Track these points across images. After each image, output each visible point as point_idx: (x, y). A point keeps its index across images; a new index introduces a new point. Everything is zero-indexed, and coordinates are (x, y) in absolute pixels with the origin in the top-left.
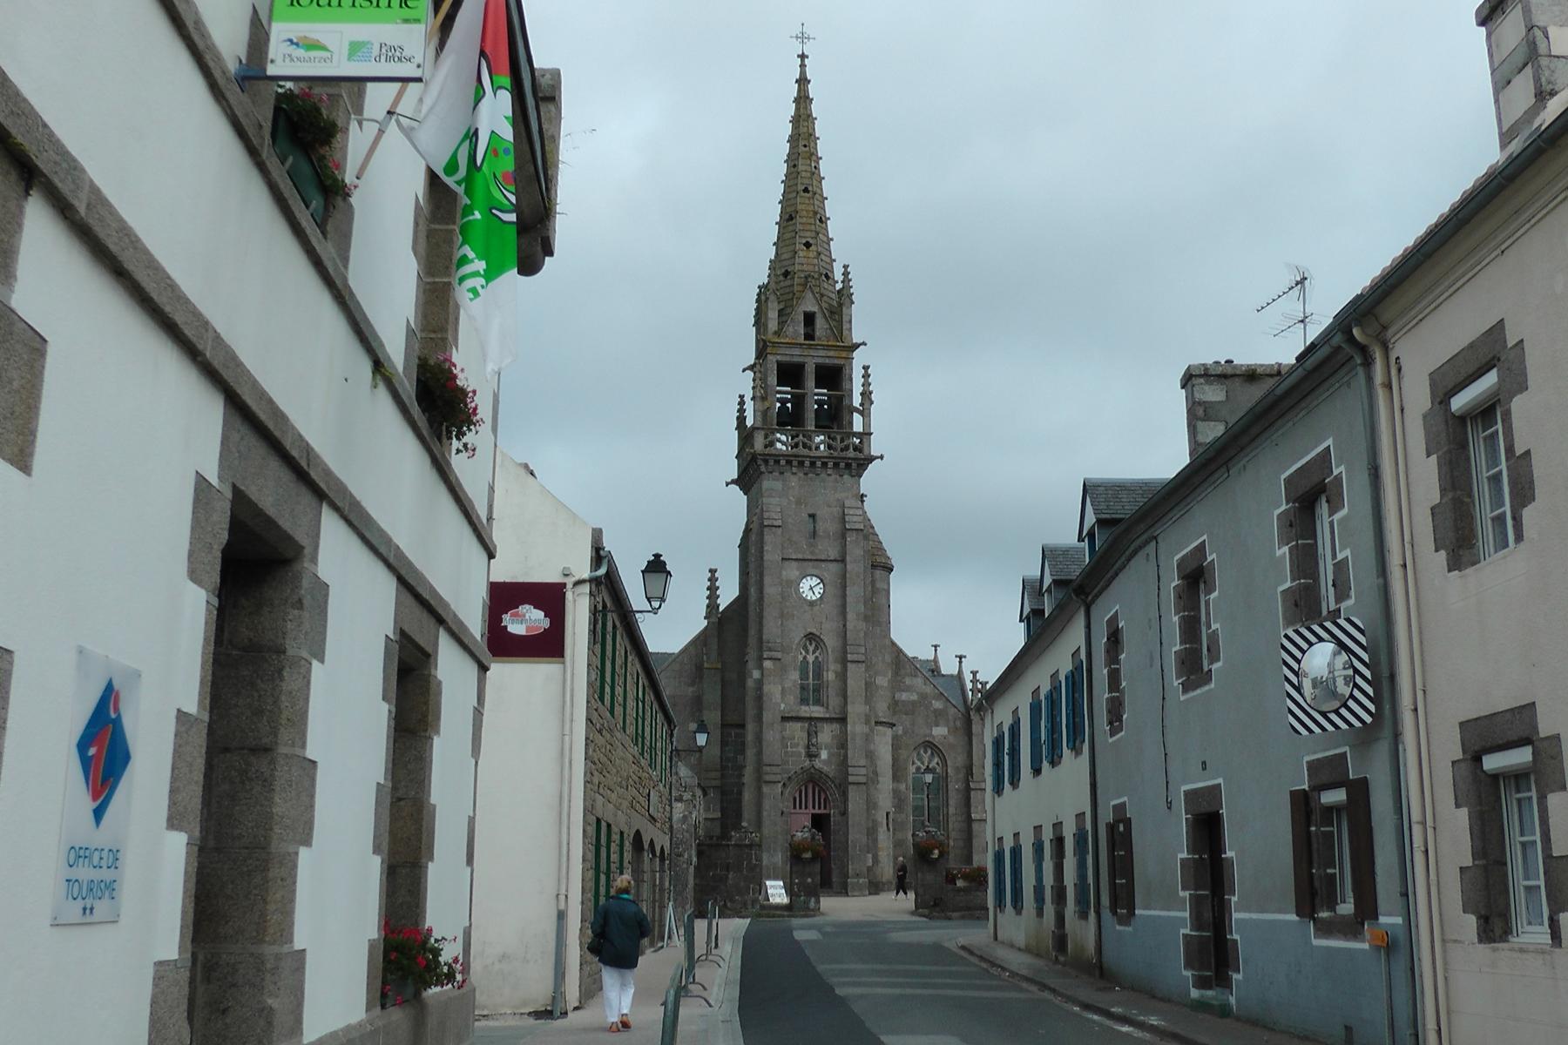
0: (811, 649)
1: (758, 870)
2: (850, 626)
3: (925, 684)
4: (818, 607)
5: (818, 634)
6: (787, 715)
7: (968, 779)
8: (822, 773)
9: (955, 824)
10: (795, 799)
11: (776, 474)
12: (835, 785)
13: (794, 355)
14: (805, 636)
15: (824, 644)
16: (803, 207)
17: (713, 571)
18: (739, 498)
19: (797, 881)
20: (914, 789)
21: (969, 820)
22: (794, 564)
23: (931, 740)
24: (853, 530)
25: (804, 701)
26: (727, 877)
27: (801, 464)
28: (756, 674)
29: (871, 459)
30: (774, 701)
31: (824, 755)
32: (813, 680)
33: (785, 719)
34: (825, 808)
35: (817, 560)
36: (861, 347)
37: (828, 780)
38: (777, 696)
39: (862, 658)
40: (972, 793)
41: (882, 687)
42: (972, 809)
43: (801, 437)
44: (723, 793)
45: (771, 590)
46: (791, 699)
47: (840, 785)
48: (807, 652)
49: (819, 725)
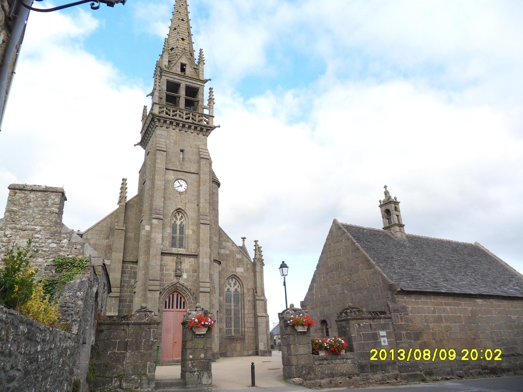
0: (179, 217)
1: (155, 348)
2: (201, 205)
3: (232, 246)
4: (184, 195)
5: (183, 209)
6: (164, 252)
8: (183, 286)
9: (249, 319)
10: (166, 302)
11: (164, 128)
12: (191, 294)
13: (175, 79)
14: (176, 210)
15: (187, 214)
18: (141, 152)
19: (191, 357)
21: (256, 317)
22: (172, 172)
23: (235, 274)
24: (204, 158)
25: (173, 245)
26: (124, 357)
27: (178, 124)
28: (147, 228)
29: (213, 128)
30: (157, 242)
31: (185, 276)
32: (180, 234)
33: (163, 254)
34: (184, 308)
35: (183, 172)
36: (217, 128)
38: (159, 241)
39: (208, 222)
40: (257, 302)
42: (258, 311)
43: (178, 112)
44: (120, 301)
45: (159, 183)
46: (167, 243)
47: (194, 293)
48: (177, 219)
49: (182, 258)
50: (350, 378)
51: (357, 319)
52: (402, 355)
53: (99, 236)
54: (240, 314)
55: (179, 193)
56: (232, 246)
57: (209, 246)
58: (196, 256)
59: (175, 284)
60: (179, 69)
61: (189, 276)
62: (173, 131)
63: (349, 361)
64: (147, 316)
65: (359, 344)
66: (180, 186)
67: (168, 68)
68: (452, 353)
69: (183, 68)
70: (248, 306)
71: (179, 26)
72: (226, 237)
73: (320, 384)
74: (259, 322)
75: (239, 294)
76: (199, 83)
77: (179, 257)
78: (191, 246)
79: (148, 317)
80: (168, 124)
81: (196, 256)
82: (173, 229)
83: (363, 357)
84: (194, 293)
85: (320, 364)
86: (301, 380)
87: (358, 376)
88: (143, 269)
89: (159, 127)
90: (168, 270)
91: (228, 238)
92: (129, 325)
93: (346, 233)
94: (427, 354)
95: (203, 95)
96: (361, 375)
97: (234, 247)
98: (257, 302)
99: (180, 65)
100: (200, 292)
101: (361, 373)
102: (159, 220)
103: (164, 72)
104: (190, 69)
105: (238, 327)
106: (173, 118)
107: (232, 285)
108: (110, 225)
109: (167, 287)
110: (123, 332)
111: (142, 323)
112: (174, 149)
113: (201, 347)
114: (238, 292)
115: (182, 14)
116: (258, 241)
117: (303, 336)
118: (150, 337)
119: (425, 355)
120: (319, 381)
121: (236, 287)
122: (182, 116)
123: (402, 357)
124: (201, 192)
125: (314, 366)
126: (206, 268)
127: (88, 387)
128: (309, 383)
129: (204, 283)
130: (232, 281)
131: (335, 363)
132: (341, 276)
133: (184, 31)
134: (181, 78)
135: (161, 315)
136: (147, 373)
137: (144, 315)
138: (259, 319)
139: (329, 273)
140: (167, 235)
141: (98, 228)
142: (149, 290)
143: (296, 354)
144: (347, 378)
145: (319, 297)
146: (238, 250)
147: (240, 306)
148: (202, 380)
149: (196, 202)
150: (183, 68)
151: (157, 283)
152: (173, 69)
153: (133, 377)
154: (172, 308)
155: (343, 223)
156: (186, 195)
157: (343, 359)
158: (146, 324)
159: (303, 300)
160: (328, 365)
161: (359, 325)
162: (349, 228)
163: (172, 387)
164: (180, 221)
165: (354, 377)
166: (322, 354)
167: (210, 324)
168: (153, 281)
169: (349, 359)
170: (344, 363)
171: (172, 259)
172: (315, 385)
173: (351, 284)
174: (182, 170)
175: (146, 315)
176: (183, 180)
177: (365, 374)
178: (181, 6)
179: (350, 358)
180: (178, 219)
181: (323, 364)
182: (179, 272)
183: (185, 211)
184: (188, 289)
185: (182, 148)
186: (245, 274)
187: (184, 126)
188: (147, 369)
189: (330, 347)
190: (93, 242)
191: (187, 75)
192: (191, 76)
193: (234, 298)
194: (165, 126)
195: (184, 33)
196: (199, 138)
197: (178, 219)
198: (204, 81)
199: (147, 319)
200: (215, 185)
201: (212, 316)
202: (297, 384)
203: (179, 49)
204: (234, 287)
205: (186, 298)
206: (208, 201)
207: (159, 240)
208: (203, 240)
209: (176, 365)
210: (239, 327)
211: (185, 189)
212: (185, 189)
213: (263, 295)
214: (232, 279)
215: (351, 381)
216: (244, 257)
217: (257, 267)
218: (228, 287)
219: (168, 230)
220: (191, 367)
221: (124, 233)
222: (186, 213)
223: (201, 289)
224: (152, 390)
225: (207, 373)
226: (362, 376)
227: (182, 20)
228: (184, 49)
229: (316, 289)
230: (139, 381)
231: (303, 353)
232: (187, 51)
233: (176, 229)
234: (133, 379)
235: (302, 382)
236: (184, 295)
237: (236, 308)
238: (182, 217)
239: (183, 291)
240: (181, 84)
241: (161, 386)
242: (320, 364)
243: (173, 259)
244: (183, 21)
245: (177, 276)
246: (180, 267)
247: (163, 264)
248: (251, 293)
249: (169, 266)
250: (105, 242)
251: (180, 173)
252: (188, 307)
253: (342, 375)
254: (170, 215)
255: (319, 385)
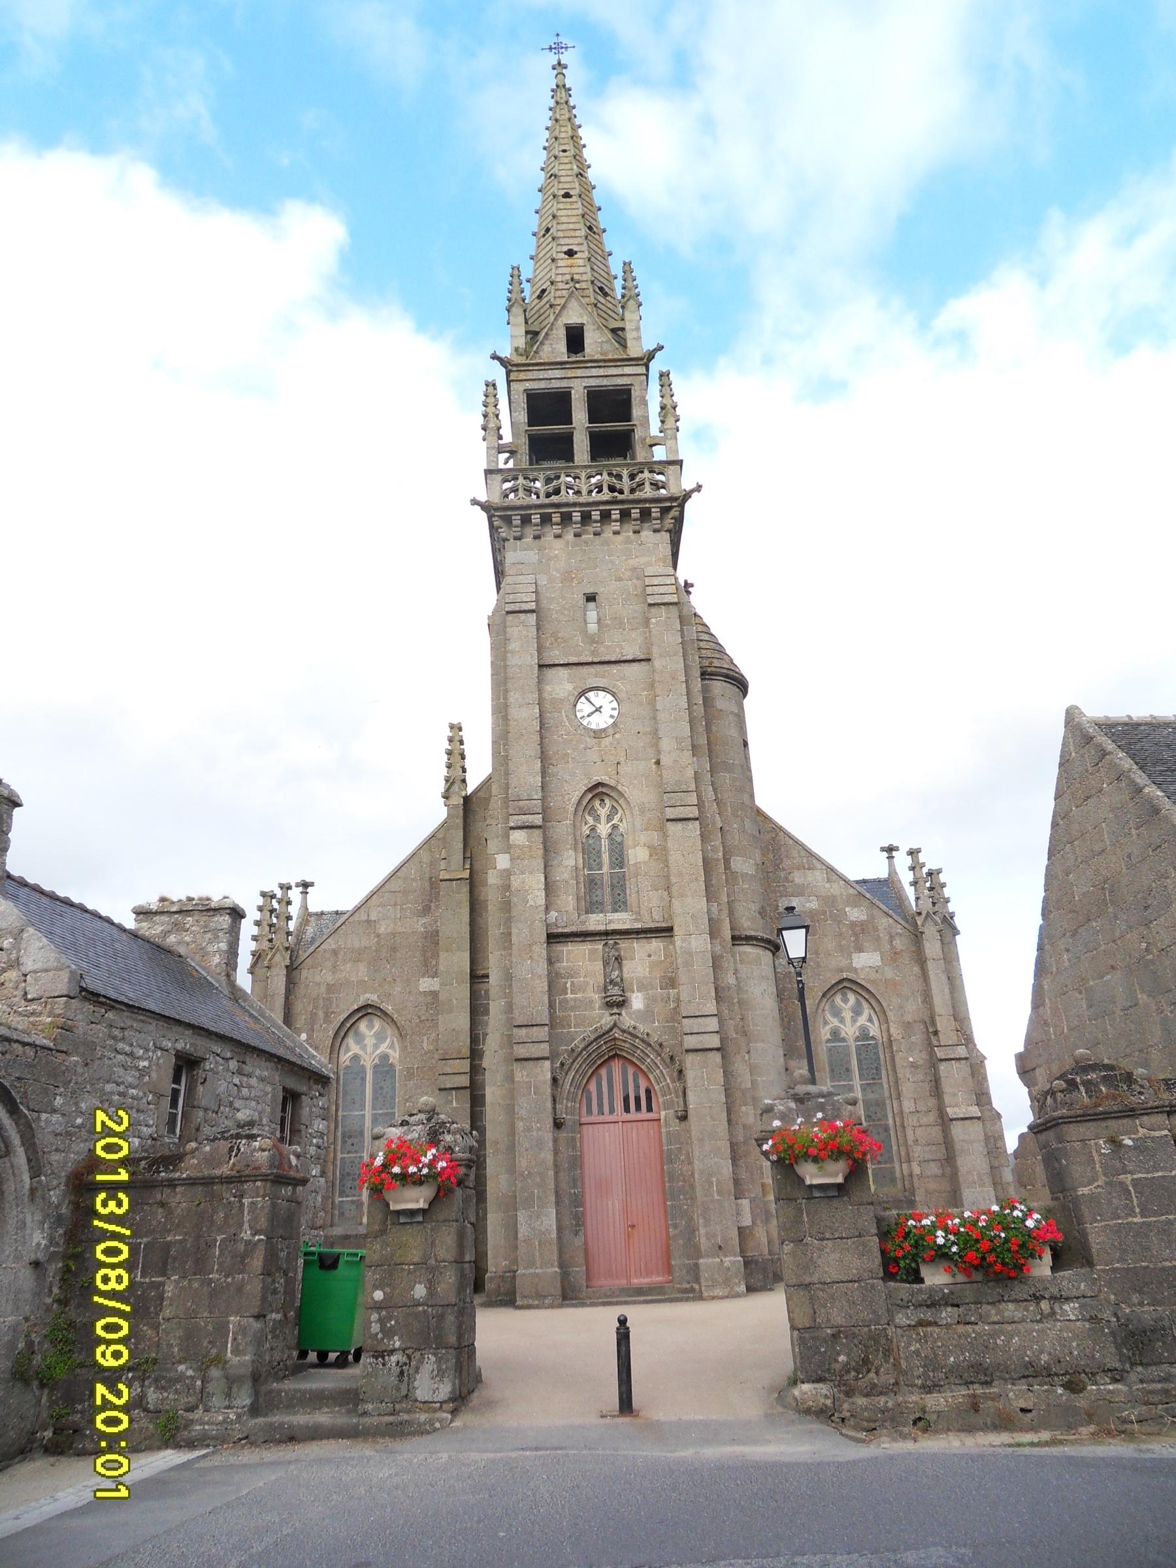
0: (603, 812)
3: (829, 881)
5: (612, 783)
7: (930, 1045)
11: (528, 540)
12: (662, 1059)
14: (590, 790)
16: (581, 270)
17: (456, 728)
19: (378, 1295)
20: (832, 1071)
22: (563, 672)
23: (852, 976)
25: (593, 907)
27: (566, 519)
28: (503, 861)
30: (531, 903)
31: (637, 1001)
32: (612, 867)
33: (553, 938)
34: (650, 1109)
36: (695, 495)
37: (648, 1050)
40: (943, 1067)
41: (744, 876)
42: (947, 1099)
46: (568, 901)
47: (672, 1058)
48: (597, 819)
49: (624, 944)
50: (1073, 1387)
51: (1106, 1116)
52: (112, 1204)
53: (402, 909)
54: (890, 1116)
55: (592, 734)
56: (829, 881)
57: (704, 893)
58: (666, 932)
59: (608, 1032)
60: (562, 347)
61: (650, 1001)
62: (559, 543)
63: (1066, 1307)
64: (234, 1154)
65: (1118, 1230)
66: (596, 710)
67: (526, 354)
68: (117, 1355)
69: (575, 339)
70: (912, 1086)
71: (554, 217)
72: (803, 853)
73: (917, 1415)
74: (955, 1138)
75: (876, 1046)
76: (627, 370)
77: (611, 942)
78: (649, 900)
79: (236, 1156)
80: (537, 525)
81: (666, 932)
82: (620, 856)
83: (1141, 1292)
84: (672, 1058)
85: (921, 1323)
86: (824, 1392)
87: (1115, 1381)
88: (501, 994)
89: (512, 540)
90: (582, 988)
91: (811, 854)
92: (175, 1186)
93: (1110, 753)
94: (113, 1279)
95: (646, 405)
96: (1133, 1377)
97: (835, 885)
98: (943, 1067)
99: (562, 333)
100: (687, 1051)
101: (1133, 1364)
102: (531, 831)
103: (515, 369)
104: (597, 335)
105: (886, 1163)
106: (547, 501)
107: (848, 1015)
108: (430, 871)
109: (581, 1046)
110: (160, 1210)
111: (213, 1178)
112: (563, 598)
113: (416, 1260)
114: (873, 1038)
115: (562, 179)
116: (919, 851)
117: (835, 1203)
118: (241, 1225)
119: (112, 1274)
120: (914, 1398)
121: (862, 1020)
122: (576, 488)
123: (105, 1204)
124: (661, 716)
125: (890, 1331)
126: (703, 968)
127: (48, 1401)
128: (866, 1409)
129: (699, 1020)
130: (846, 1001)
131: (995, 1319)
132: (1117, 934)
133: (571, 226)
134: (569, 371)
135: (574, 1139)
136: (229, 1355)
137: (226, 1150)
138: (957, 1130)
139: (1080, 931)
140: (566, 876)
141: (394, 885)
142: (517, 1060)
143: (808, 1280)
144: (1060, 1391)
145: (1066, 1030)
146: (852, 891)
147: (886, 1086)
148: (416, 1384)
149: (651, 752)
150: (575, 339)
151: (542, 1034)
152: (541, 353)
153: (181, 1368)
154: (612, 1111)
155: (1156, 714)
156: (617, 736)
157: (1037, 1298)
158: (227, 1180)
159: (1021, 1048)
160: (961, 1329)
161: (1114, 1142)
162: (1108, 727)
163: (320, 1409)
164: (610, 824)
165: (1096, 1383)
166: (936, 1278)
167: (425, 1171)
168: (529, 1030)
169: (1068, 1299)
170: (1043, 1318)
171: (589, 950)
172: (892, 1419)
173: (1151, 961)
174: (596, 660)
175: (231, 1149)
176: (604, 689)
177: (1154, 1371)
178: (562, 154)
179: (1075, 1293)
180: (603, 819)
181: (936, 1324)
182: (616, 991)
183: (619, 788)
184: (650, 1045)
185: (590, 590)
186: (889, 973)
187: (586, 518)
188: (230, 1340)
189: (961, 1250)
190: (386, 929)
191: (589, 355)
192: (601, 354)
193: (859, 1061)
194: (530, 531)
195: (572, 234)
196: (642, 544)
197: (603, 819)
198: (641, 359)
199: (232, 1161)
200: (718, 687)
201: (455, 1141)
202: (808, 1411)
203: (561, 286)
204: (854, 1021)
205: (651, 1077)
206: (688, 743)
207: (539, 893)
208: (680, 874)
209: (634, 1303)
210: (892, 1161)
211: (612, 716)
212: (612, 716)
213: (967, 1039)
214: (844, 995)
215: (1081, 1402)
216: (876, 912)
217: (927, 945)
218: (831, 1025)
219: (568, 858)
220: (380, 1336)
221: (466, 889)
222: (621, 794)
223: (691, 1042)
224: (239, 1416)
225: (433, 1358)
226: (1142, 1381)
227: (567, 195)
228: (572, 279)
229: (1050, 1000)
230: (199, 1383)
231: (836, 1277)
232: (584, 285)
233: (599, 852)
234: (181, 1378)
235: (829, 1402)
236: (643, 1067)
237: (871, 1096)
238: (614, 809)
239: (639, 1052)
240: (573, 392)
241: (281, 1402)
242: (921, 1323)
243: (595, 951)
244: (568, 200)
245: (609, 1005)
246: (616, 973)
247: (562, 971)
248: (918, 1038)
249: (582, 973)
250: (420, 924)
251: (586, 669)
252: (662, 1106)
253: (1033, 1373)
254: (571, 809)
255: (912, 1417)
